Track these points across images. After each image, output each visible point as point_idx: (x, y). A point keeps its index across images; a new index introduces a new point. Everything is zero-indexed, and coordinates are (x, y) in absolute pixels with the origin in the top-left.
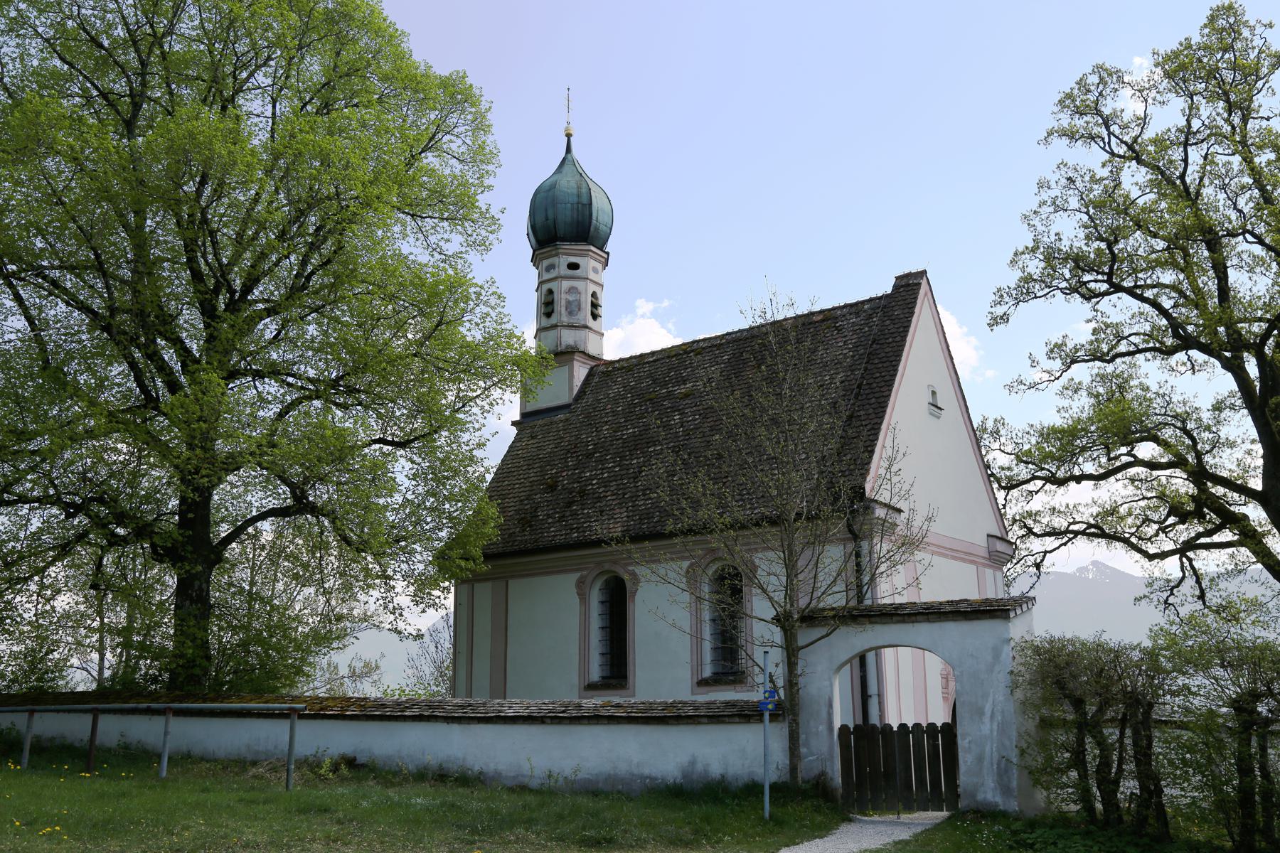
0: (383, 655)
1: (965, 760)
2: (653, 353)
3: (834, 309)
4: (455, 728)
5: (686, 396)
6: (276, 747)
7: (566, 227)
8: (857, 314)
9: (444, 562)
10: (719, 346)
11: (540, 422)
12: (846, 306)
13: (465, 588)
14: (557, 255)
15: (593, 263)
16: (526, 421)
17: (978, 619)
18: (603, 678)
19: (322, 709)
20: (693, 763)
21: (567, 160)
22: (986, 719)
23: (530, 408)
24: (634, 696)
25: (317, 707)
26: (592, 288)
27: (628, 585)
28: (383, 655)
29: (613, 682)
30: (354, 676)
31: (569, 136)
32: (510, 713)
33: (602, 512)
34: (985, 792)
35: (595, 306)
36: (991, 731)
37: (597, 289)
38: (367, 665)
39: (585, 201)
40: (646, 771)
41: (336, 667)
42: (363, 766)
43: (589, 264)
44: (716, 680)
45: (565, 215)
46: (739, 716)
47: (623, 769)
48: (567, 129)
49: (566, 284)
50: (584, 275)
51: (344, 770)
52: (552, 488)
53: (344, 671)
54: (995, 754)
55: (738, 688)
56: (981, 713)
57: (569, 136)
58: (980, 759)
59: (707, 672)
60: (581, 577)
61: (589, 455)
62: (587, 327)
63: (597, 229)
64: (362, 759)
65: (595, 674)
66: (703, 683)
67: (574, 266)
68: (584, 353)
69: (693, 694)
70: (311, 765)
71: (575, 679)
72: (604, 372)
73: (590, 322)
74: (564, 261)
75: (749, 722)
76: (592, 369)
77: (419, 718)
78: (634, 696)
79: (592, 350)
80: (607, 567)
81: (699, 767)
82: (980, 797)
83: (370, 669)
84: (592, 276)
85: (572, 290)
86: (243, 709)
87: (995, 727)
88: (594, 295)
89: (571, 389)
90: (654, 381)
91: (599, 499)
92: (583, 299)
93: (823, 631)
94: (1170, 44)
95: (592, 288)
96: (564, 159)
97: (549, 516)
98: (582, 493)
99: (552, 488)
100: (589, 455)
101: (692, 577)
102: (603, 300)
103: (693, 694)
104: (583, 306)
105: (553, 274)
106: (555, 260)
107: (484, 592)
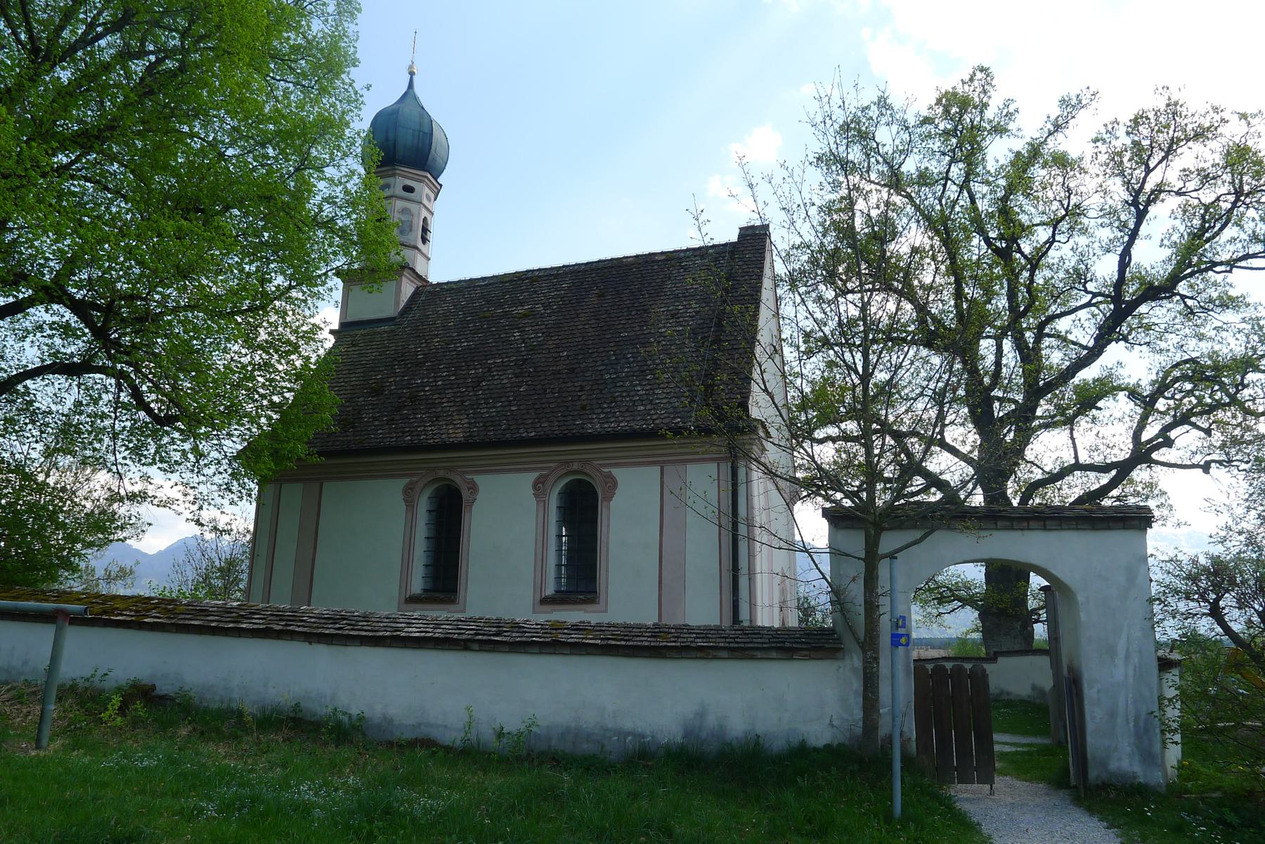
0: (138, 563)
1: (1094, 715)
2: (484, 279)
3: (675, 251)
4: (322, 650)
5: (525, 316)
6: (25, 663)
7: (406, 150)
8: (702, 257)
9: (249, 459)
10: (556, 276)
11: (362, 332)
12: (688, 250)
13: (270, 489)
14: (394, 175)
15: (427, 190)
16: (346, 330)
17: (1109, 528)
18: (425, 590)
19: (105, 612)
20: (701, 714)
21: (409, 93)
22: (1120, 661)
23: (349, 319)
24: (463, 611)
25: (98, 608)
26: (424, 213)
27: (465, 494)
28: (138, 563)
29: (441, 596)
30: (109, 578)
31: (412, 74)
32: (414, 632)
33: (438, 417)
34: (1120, 759)
35: (425, 230)
36: (1126, 676)
37: (428, 216)
38: (122, 569)
39: (426, 130)
40: (628, 725)
41: (93, 570)
42: (163, 698)
43: (424, 190)
44: (559, 599)
45: (406, 139)
46: (778, 649)
47: (589, 720)
48: (411, 67)
49: (400, 204)
50: (418, 199)
51: (139, 707)
52: (377, 391)
53: (100, 573)
54: (1131, 707)
55: (451, 607)
56: (1112, 651)
57: (412, 74)
58: (1112, 714)
59: (550, 590)
60: (410, 483)
61: (419, 364)
62: (417, 248)
63: (434, 160)
64: (163, 688)
65: (417, 585)
66: (546, 601)
67: (409, 189)
68: (413, 270)
69: (534, 612)
70: (87, 698)
71: (394, 590)
72: (429, 294)
73: (420, 245)
74: (400, 182)
75: (791, 659)
76: (417, 288)
77: (266, 633)
78: (463, 611)
79: (419, 270)
80: (441, 473)
81: (711, 721)
82: (1113, 766)
83: (123, 574)
84: (425, 201)
85: (404, 211)
86: (16, 609)
87: (1131, 672)
88: (425, 219)
89: (397, 303)
90: (488, 302)
91: (434, 405)
92: (415, 221)
93: (918, 534)
94: (947, 86)
95: (424, 213)
96: (406, 93)
97: (375, 419)
98: (413, 398)
99: (377, 391)
100: (419, 364)
101: (539, 487)
102: (434, 226)
103: (534, 612)
104: (414, 227)
105: (387, 193)
106: (391, 180)
107: (293, 494)
